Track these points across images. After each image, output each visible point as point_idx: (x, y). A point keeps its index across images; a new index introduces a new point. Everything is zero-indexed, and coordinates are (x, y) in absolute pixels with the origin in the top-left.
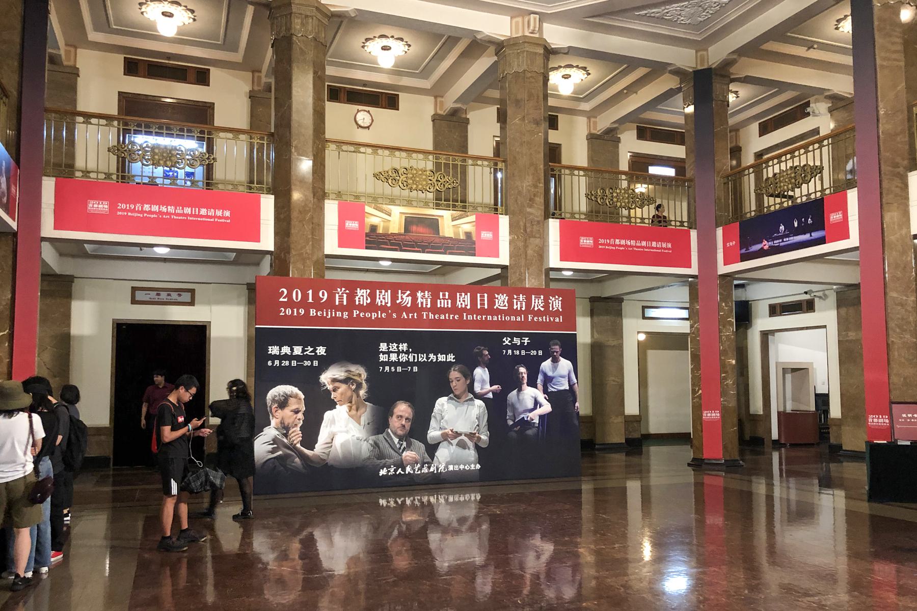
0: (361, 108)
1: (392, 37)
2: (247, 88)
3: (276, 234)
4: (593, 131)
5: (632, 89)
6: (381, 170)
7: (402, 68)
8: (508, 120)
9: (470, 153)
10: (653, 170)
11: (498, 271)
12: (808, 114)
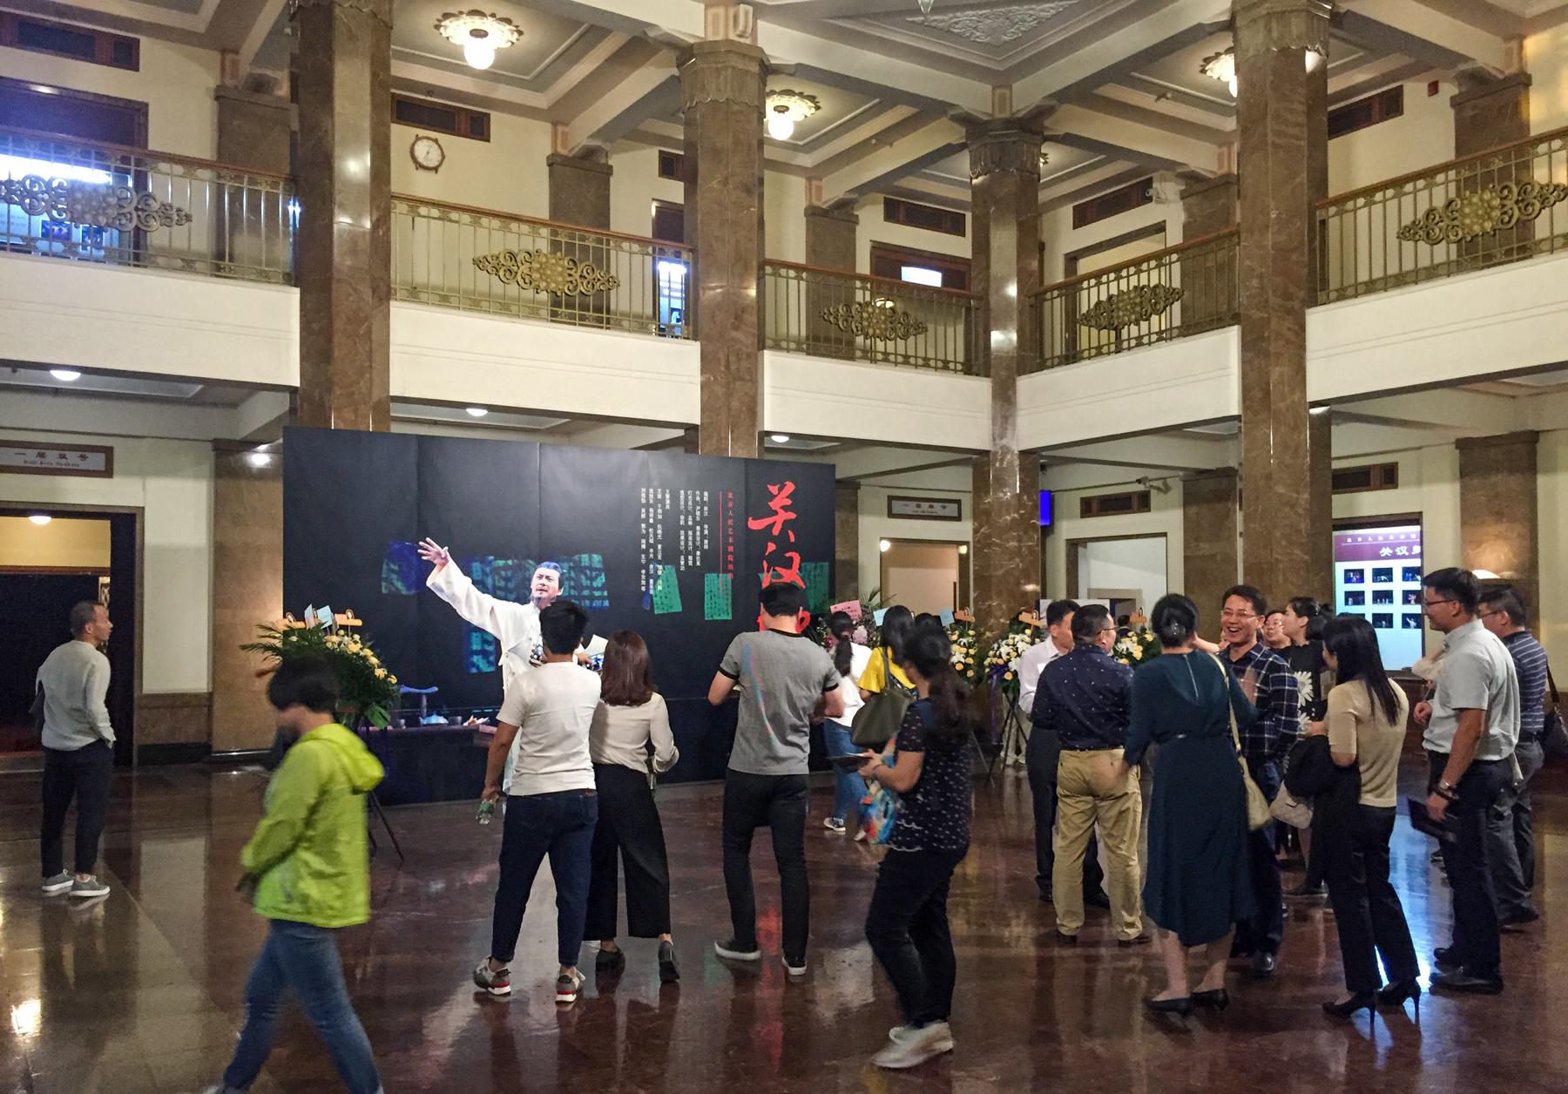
0: (422, 132)
1: (493, 15)
2: (212, 82)
3: (304, 358)
4: (816, 203)
5: (885, 138)
6: (486, 253)
7: (506, 69)
8: (700, 181)
9: (613, 228)
10: (911, 274)
11: (680, 433)
12: (1150, 199)
